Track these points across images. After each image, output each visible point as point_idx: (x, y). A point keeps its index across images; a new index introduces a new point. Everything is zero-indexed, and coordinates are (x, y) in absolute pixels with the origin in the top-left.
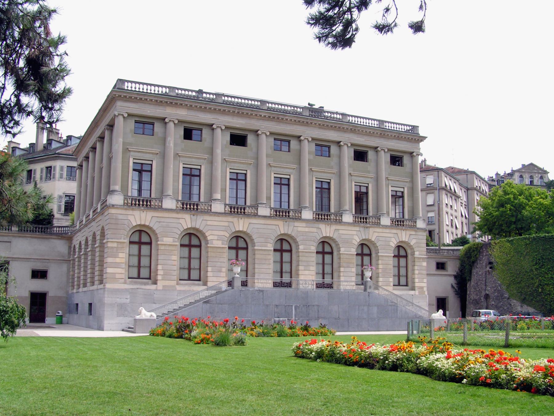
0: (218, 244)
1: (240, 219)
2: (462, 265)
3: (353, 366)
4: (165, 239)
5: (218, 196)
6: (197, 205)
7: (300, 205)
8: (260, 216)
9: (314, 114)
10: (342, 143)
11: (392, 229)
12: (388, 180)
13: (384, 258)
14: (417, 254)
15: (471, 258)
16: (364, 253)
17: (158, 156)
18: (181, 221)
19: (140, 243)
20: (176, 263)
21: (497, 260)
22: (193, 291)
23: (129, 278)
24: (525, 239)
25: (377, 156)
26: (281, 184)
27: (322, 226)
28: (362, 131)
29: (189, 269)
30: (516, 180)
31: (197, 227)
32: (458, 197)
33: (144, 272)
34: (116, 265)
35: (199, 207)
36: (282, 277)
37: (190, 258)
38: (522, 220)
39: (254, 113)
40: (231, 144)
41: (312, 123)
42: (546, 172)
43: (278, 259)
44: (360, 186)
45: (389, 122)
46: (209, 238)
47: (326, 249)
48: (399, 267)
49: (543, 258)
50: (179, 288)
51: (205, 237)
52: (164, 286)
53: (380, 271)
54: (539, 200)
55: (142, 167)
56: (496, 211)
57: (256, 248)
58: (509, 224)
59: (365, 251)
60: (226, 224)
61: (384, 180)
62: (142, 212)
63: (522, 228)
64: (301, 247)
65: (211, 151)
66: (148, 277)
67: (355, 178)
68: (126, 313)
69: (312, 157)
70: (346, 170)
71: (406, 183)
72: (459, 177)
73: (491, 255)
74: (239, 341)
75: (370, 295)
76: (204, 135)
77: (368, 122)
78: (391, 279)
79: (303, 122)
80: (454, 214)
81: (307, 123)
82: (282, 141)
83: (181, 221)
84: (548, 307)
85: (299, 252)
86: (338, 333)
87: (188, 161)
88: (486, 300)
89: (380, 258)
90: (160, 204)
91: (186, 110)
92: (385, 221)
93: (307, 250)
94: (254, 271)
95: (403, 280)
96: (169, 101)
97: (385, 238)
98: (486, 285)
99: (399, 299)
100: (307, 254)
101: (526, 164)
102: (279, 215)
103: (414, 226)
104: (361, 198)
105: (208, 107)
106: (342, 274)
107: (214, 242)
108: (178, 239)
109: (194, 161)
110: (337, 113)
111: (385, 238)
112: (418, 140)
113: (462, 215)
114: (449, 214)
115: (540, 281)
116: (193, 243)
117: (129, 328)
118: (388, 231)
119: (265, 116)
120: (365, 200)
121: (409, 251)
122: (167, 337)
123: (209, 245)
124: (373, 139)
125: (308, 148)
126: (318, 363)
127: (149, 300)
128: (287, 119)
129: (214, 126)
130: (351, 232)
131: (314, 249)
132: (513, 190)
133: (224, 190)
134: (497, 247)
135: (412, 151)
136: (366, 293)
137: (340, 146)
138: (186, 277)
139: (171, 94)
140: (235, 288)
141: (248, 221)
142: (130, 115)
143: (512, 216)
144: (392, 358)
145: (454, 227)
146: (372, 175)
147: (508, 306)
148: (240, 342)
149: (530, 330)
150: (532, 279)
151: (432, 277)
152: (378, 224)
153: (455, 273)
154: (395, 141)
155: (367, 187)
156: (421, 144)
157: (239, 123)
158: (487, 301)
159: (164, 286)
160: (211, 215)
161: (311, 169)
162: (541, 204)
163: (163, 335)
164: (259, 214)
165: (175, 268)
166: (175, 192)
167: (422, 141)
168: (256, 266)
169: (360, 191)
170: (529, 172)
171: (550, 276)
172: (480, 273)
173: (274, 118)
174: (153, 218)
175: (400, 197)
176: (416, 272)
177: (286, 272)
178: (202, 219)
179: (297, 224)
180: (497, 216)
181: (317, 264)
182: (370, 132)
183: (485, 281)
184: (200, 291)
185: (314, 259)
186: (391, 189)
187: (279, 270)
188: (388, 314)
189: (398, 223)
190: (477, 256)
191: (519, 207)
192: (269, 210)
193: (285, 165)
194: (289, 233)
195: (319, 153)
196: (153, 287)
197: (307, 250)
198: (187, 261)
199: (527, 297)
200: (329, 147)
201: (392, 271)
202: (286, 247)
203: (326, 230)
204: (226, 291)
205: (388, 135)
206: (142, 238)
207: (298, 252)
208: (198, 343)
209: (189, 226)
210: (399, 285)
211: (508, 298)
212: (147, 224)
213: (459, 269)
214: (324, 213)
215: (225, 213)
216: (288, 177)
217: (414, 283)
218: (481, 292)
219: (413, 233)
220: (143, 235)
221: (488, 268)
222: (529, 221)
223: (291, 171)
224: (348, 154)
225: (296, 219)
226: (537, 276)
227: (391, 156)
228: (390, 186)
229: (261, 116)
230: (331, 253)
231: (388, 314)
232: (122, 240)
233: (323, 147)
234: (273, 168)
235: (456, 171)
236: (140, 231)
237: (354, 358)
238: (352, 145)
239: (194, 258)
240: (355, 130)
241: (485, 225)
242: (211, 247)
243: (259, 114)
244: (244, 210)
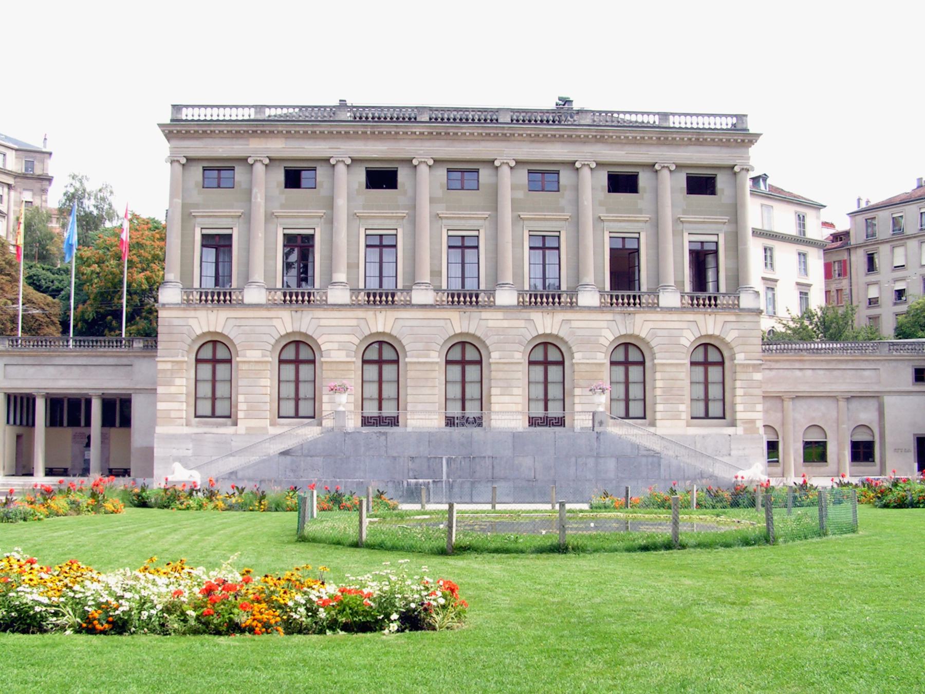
0: (341, 356)
4: (248, 353)
5: (341, 276)
6: (393, 295)
7: (658, 282)
9: (560, 119)
10: (657, 167)
11: (685, 313)
13: (668, 369)
14: (740, 358)
17: (241, 220)
18: (276, 322)
19: (626, 363)
23: (196, 416)
25: (657, 179)
29: (707, 400)
34: (172, 398)
35: (718, 302)
36: (463, 408)
37: (706, 383)
39: (401, 131)
52: (247, 429)
55: (381, 241)
60: (354, 323)
62: (210, 312)
65: (330, 203)
66: (721, 415)
67: (611, 224)
69: (520, 194)
75: (601, 437)
76: (563, 181)
82: (463, 173)
83: (276, 322)
87: (290, 222)
89: (658, 368)
90: (324, 298)
91: (283, 140)
93: (425, 362)
96: (250, 129)
100: (506, 367)
103: (734, 305)
104: (701, 260)
105: (318, 130)
107: (333, 353)
108: (523, 353)
109: (302, 223)
112: (743, 141)
116: (631, 359)
124: (643, 149)
133: (352, 266)
135: (731, 163)
139: (259, 117)
142: (518, 162)
154: (691, 148)
157: (622, 155)
159: (247, 429)
160: (325, 310)
164: (414, 302)
165: (268, 399)
166: (436, 274)
167: (751, 142)
174: (229, 321)
177: (305, 399)
178: (311, 316)
179: (486, 314)
184: (309, 432)
196: (231, 430)
197: (425, 362)
198: (701, 388)
206: (215, 354)
209: (290, 330)
212: (219, 330)
217: (734, 412)
219: (732, 318)
223: (481, 222)
232: (180, 359)
234: (444, 221)
242: (326, 362)
243: (574, 134)
244: (559, 298)
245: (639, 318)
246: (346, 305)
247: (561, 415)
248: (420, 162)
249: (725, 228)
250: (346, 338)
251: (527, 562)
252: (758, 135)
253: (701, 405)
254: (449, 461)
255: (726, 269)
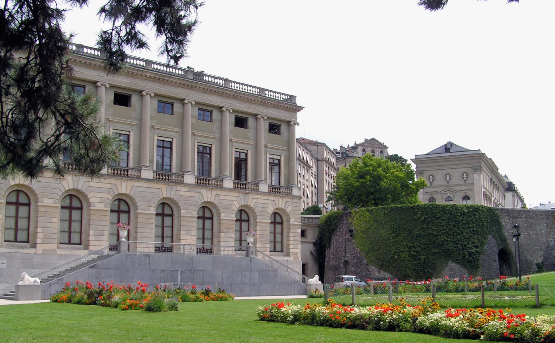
0: (101, 206)
1: (123, 181)
2: (320, 233)
3: (341, 327)
7: (182, 168)
8: (143, 179)
10: (224, 109)
12: (266, 147)
13: (262, 225)
14: (292, 221)
15: (331, 226)
16: (243, 218)
19: (17, 204)
20: (56, 226)
21: (357, 228)
22: (74, 255)
23: (5, 241)
24: (384, 209)
25: (257, 123)
26: (163, 147)
27: (204, 191)
28: (244, 98)
29: (16, 229)
30: (359, 153)
31: (79, 188)
32: (310, 167)
33: (22, 235)
36: (204, 243)
37: (70, 221)
38: (380, 190)
40: (115, 103)
41: (196, 87)
42: (386, 147)
43: (160, 223)
44: (240, 152)
45: (268, 91)
46: (91, 200)
47: (207, 214)
48: (275, 233)
49: (399, 227)
50: (59, 252)
51: (87, 199)
52: (43, 250)
53: (258, 237)
54: (395, 173)
55: (163, 144)
56: (357, 182)
57: (139, 211)
58: (369, 194)
59: (244, 217)
61: (264, 149)
63: (379, 199)
64: (183, 212)
67: (236, 144)
68: (3, 279)
69: (194, 121)
70: (228, 136)
71: (282, 152)
72: (310, 148)
73: (351, 223)
74: (173, 307)
77: (249, 89)
78: (268, 245)
79: (188, 85)
80: (306, 183)
81: (192, 86)
82: (166, 104)
84: (403, 272)
85: (181, 216)
86: (236, 298)
88: (345, 266)
89: (258, 224)
92: (264, 188)
93: (189, 214)
94: (137, 235)
95: (279, 246)
97: (263, 204)
98: (345, 252)
99: (279, 265)
100: (189, 219)
101: (369, 139)
102: (162, 179)
104: (240, 165)
106: (222, 239)
107: (97, 204)
110: (220, 78)
111: (263, 204)
112: (296, 109)
113: (312, 185)
114: (302, 183)
115: (396, 248)
116: (165, 213)
117: (5, 295)
118: (265, 197)
119: (150, 77)
120: (243, 166)
121: (285, 218)
122: (75, 303)
123: (91, 208)
124: (253, 106)
125: (191, 112)
126: (296, 326)
127: (29, 265)
128: (172, 82)
129: (99, 84)
130: (231, 198)
131: (195, 214)
132: (372, 162)
134: (357, 216)
135: (289, 120)
136: (249, 258)
137: (221, 112)
138: (67, 241)
140: (122, 252)
141: (131, 183)
143: (371, 187)
144: (387, 317)
145: (306, 196)
146: (252, 142)
147: (367, 272)
148: (173, 308)
149: (406, 294)
150: (390, 246)
151: (306, 244)
152: (256, 191)
153: (314, 241)
154: (274, 109)
155: (246, 154)
156: (298, 114)
158: (346, 267)
159: (43, 250)
161: (193, 133)
162: (397, 177)
163: (69, 301)
164: (143, 176)
165: (56, 231)
167: (299, 110)
168: (139, 230)
169: (240, 158)
170: (371, 147)
171: (405, 243)
172: (340, 241)
173: (159, 79)
175: (276, 165)
176: (292, 238)
180: (357, 186)
181: (198, 229)
182: (251, 99)
183: (345, 248)
184: (81, 255)
185: (195, 224)
186: (268, 156)
187: (160, 234)
188: (269, 279)
189: (275, 190)
190: (338, 224)
191: (379, 178)
192: (152, 173)
193: (168, 128)
194: (172, 197)
195: (202, 117)
196: (32, 251)
197: (189, 214)
198: (67, 223)
199: (385, 263)
200: (211, 112)
201: (269, 237)
202: (167, 211)
203: (208, 195)
204: (109, 256)
205: (268, 103)
207: (180, 216)
208: (126, 309)
209: (71, 187)
210: (275, 251)
211: (367, 265)
213: (318, 237)
214: (205, 178)
215: (108, 175)
216: (171, 140)
218: (340, 259)
219: (289, 200)
220: (21, 195)
221: (348, 236)
222: (387, 192)
223: (174, 134)
224: (229, 119)
225: (178, 183)
226: (394, 244)
227: (269, 124)
228: (268, 154)
229: (146, 76)
230: (211, 218)
231: (269, 279)
233: (206, 112)
234: (156, 131)
235: (307, 142)
236: (18, 191)
237: (341, 319)
238: (234, 111)
239: (75, 221)
240: (237, 96)
241: (346, 195)
242: (93, 209)
245: (250, 196)
246: (229, 189)
247: (170, 246)
248: (147, 94)
249: (284, 153)
250: (105, 195)
251: (282, 326)
252: (302, 108)
253: (12, 233)
254: (181, 272)
255: (284, 174)
